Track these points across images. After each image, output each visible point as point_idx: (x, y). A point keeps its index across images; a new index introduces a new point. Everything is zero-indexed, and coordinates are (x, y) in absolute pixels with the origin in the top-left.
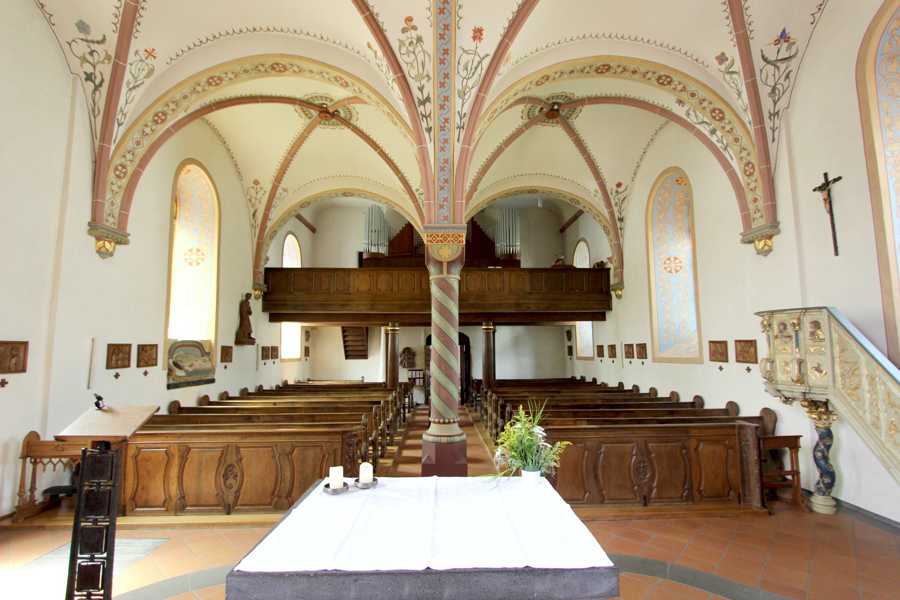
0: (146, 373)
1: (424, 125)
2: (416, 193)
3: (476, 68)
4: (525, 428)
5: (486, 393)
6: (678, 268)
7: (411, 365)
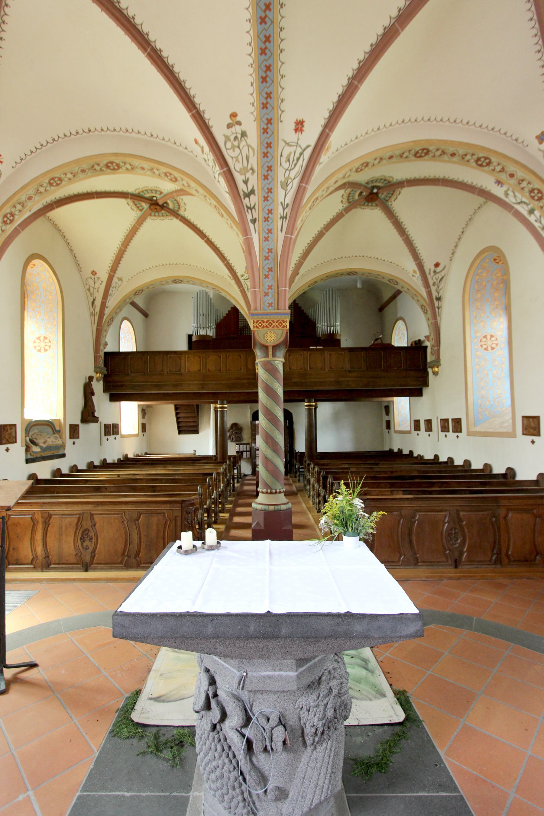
0: (7, 450)
1: (249, 217)
2: (241, 279)
3: (298, 159)
4: (345, 500)
5: (309, 465)
6: (494, 346)
7: (238, 440)
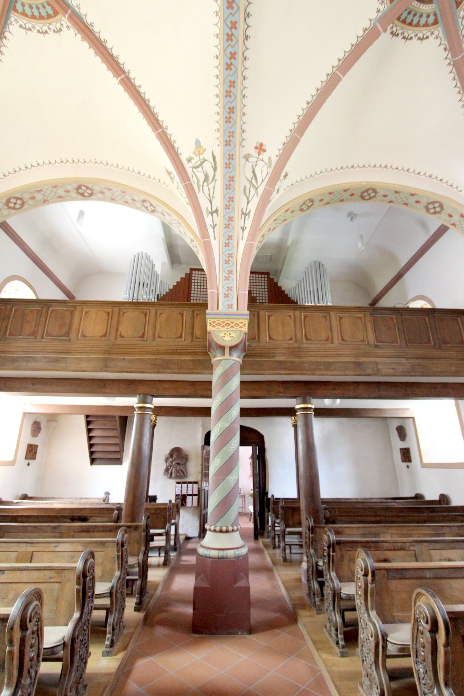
2: (188, 166)
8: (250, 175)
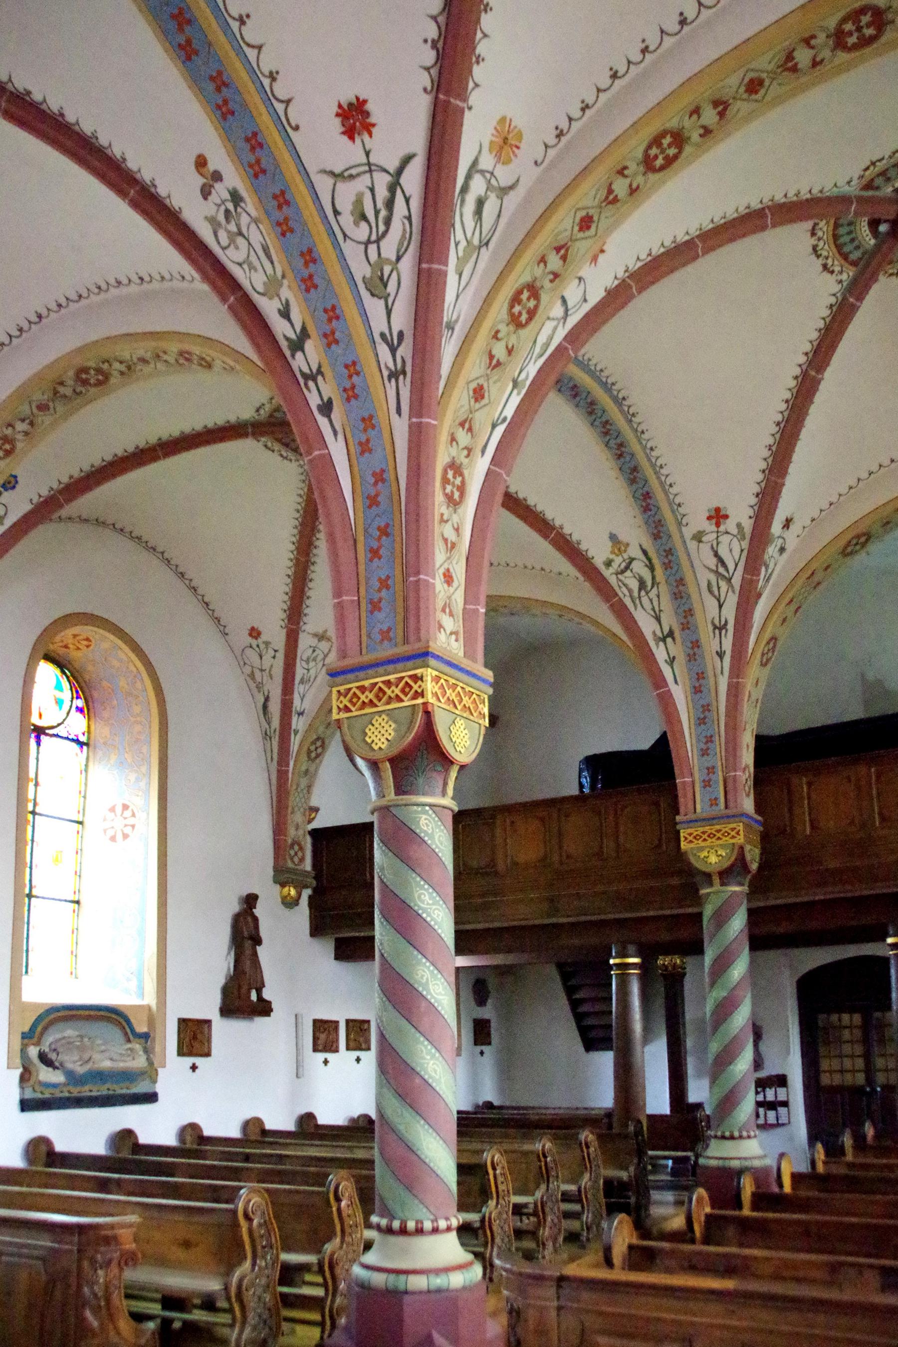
2: (608, 573)
3: (390, 204)
8: (712, 562)
